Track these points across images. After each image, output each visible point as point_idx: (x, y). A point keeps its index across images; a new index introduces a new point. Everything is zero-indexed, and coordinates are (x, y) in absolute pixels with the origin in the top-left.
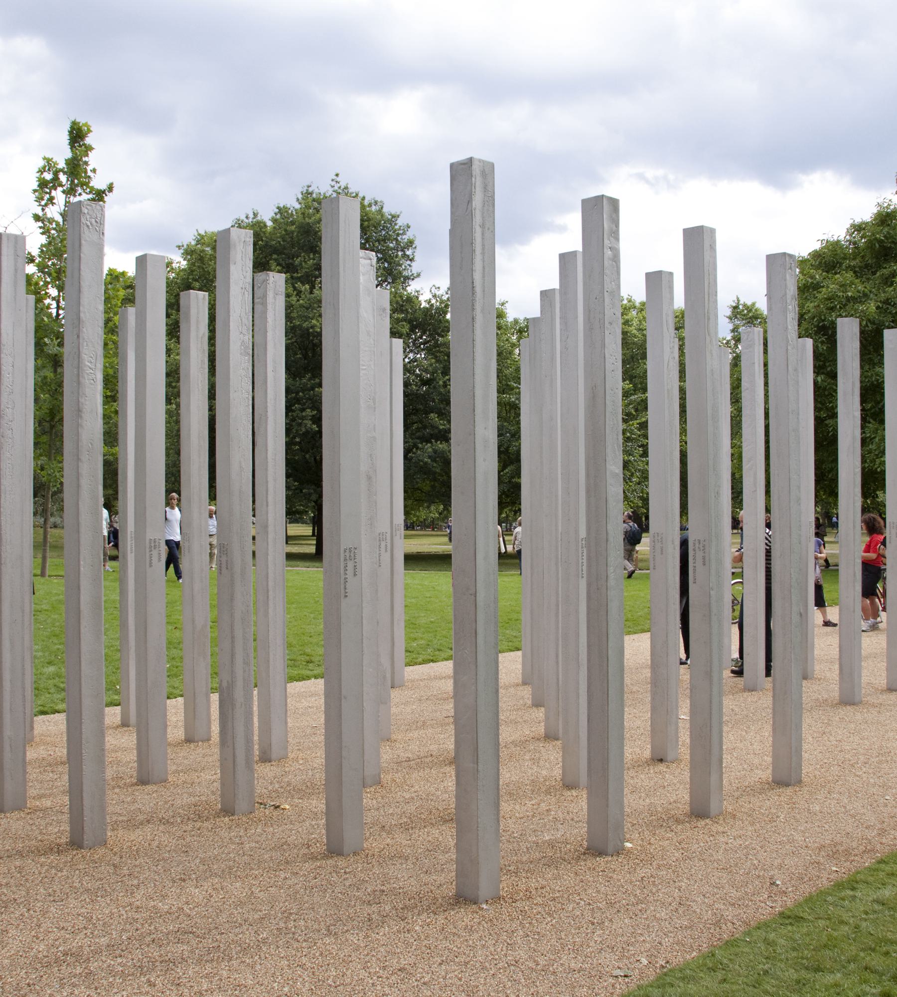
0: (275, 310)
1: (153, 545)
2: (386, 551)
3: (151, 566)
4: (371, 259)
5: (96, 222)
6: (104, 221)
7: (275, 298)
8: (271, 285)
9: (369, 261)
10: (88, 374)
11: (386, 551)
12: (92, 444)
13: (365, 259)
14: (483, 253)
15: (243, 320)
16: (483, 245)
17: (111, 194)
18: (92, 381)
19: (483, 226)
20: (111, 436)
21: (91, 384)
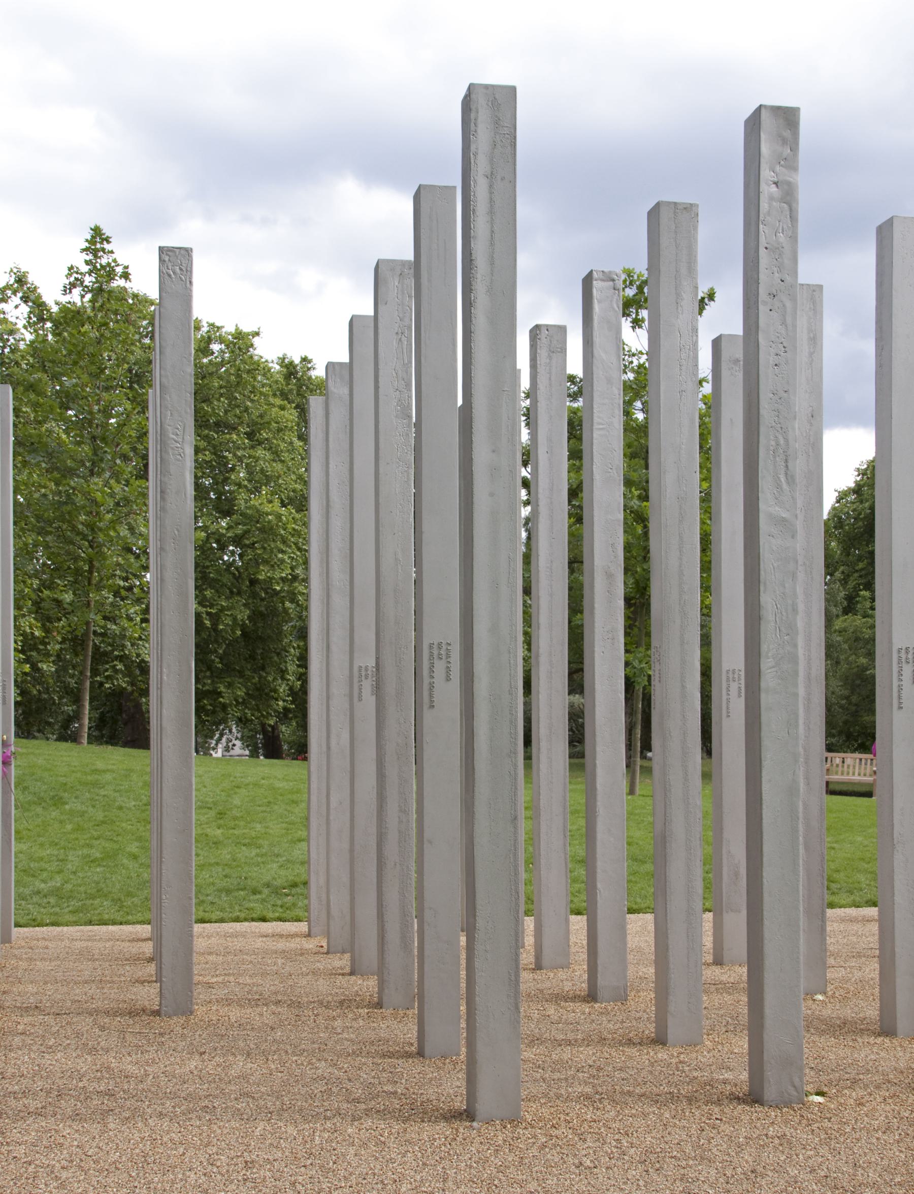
0: (550, 373)
1: (363, 673)
2: (448, 679)
3: (360, 699)
4: (613, 280)
5: (181, 269)
6: (191, 268)
7: (550, 358)
8: (544, 340)
9: (611, 283)
10: (172, 448)
11: (448, 679)
12: (178, 530)
13: (603, 280)
14: (491, 212)
15: (400, 372)
16: (491, 201)
17: (712, 303)
18: (179, 457)
19: (491, 177)
20: (576, 563)
21: (179, 460)
